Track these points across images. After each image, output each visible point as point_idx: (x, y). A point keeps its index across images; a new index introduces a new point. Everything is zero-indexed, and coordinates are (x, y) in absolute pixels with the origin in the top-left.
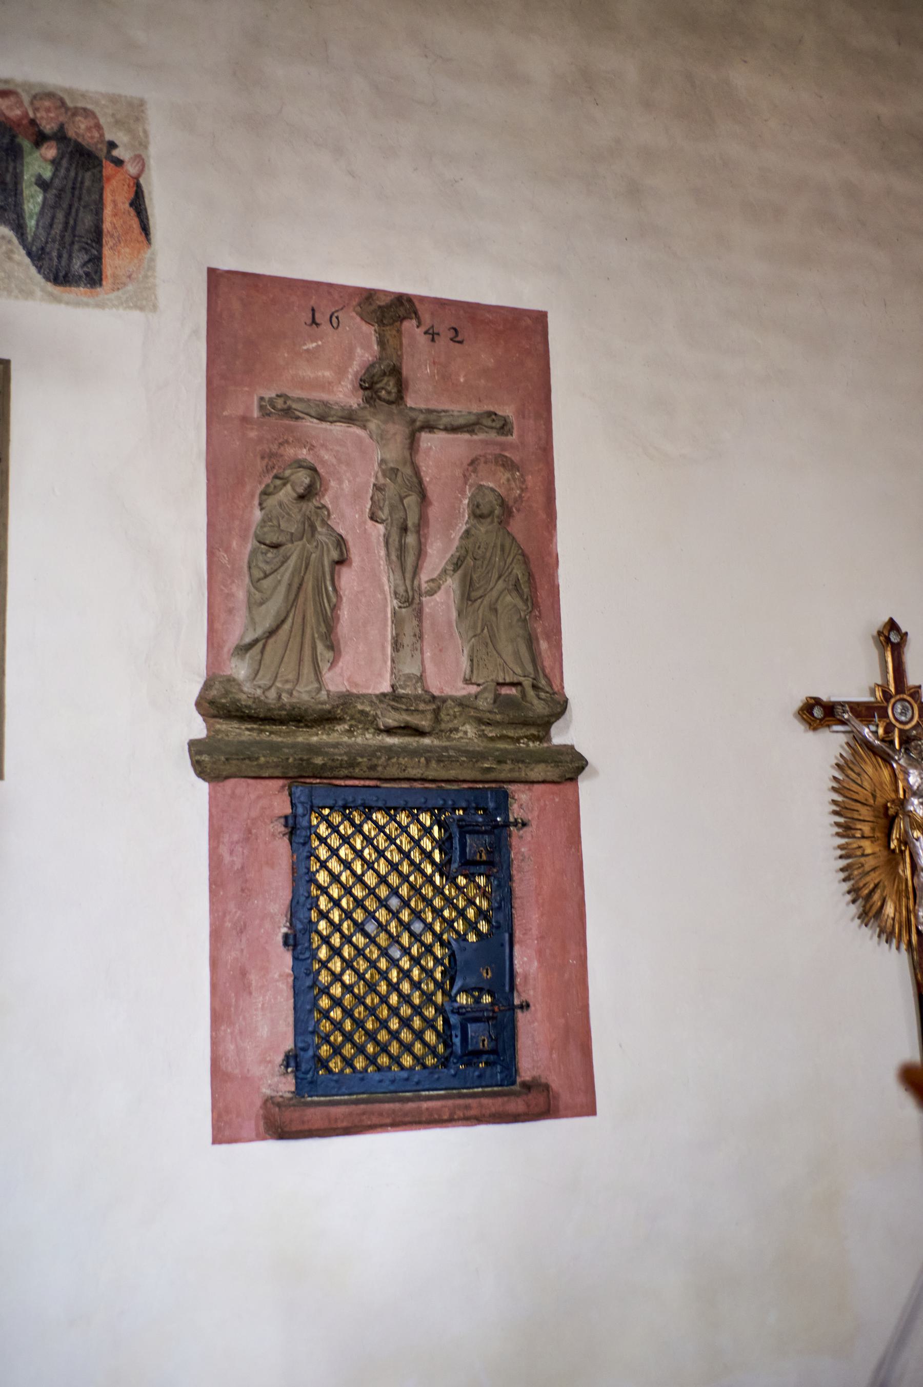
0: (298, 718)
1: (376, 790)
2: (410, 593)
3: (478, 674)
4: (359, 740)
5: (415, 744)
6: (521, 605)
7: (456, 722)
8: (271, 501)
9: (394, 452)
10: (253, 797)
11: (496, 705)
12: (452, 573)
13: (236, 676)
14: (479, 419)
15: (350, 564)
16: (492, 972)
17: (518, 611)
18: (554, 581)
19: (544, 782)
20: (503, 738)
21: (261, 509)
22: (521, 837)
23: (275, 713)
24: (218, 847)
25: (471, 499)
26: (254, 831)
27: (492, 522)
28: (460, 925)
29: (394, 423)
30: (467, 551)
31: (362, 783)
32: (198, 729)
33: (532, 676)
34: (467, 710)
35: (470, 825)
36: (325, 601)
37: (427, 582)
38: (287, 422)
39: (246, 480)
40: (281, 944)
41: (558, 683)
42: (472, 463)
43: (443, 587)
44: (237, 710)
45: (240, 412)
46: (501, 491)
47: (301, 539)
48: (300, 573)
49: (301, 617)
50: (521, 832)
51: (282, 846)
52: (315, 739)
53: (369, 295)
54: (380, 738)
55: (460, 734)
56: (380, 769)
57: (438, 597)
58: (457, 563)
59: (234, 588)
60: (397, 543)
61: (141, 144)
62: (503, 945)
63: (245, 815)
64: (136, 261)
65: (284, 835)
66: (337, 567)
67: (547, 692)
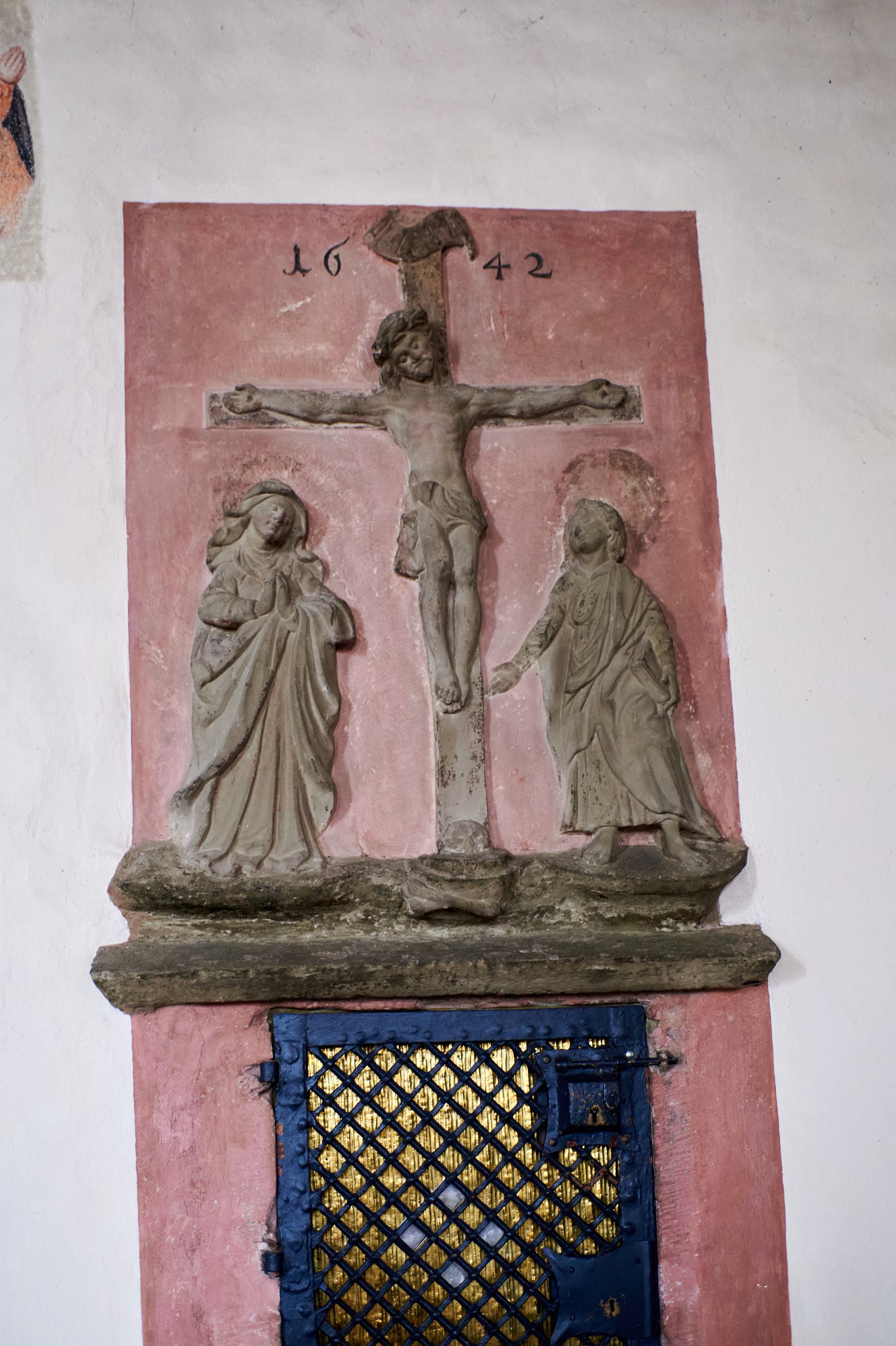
0: (267, 904)
1: (416, 1015)
2: (464, 688)
3: (586, 814)
4: (384, 935)
5: (477, 938)
6: (655, 692)
7: (546, 896)
8: (225, 556)
9: (431, 454)
10: (207, 1033)
11: (615, 865)
12: (538, 650)
13: (176, 842)
14: (578, 394)
15: (365, 648)
16: (621, 1308)
17: (653, 703)
18: (719, 651)
19: (705, 989)
20: (630, 919)
21: (212, 570)
22: (668, 1083)
23: (228, 897)
24: (150, 1117)
25: (568, 526)
26: (209, 1090)
27: (604, 559)
28: (567, 1229)
29: (427, 408)
30: (563, 613)
31: (390, 1005)
32: (115, 928)
33: (678, 811)
34: (563, 875)
35: (577, 1067)
36: (314, 708)
37: (496, 669)
38: (257, 431)
39: (191, 527)
40: (260, 1268)
41: (731, 821)
42: (571, 467)
43: (524, 676)
44: (165, 897)
45: (180, 422)
46: (624, 512)
47: (271, 608)
48: (267, 664)
49: (273, 738)
50: (668, 1075)
51: (258, 1113)
52: (308, 936)
53: (389, 216)
54: (418, 930)
55: (559, 918)
56: (409, 981)
57: (515, 693)
58: (548, 635)
59: (174, 702)
60: (435, 604)
61: (19, 30)
62: (638, 1261)
63: (195, 1065)
64: (10, 206)
65: (261, 1093)
66: (340, 656)
67: (710, 839)
